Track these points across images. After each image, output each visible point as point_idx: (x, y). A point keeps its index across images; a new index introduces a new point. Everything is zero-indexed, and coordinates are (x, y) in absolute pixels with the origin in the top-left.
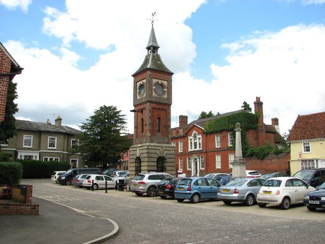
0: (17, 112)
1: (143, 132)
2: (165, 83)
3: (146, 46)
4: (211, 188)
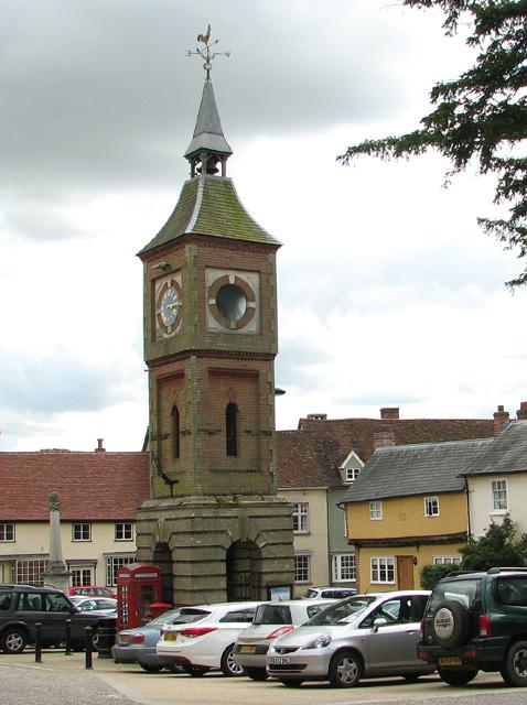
0: (396, 411)
1: (177, 455)
2: (252, 280)
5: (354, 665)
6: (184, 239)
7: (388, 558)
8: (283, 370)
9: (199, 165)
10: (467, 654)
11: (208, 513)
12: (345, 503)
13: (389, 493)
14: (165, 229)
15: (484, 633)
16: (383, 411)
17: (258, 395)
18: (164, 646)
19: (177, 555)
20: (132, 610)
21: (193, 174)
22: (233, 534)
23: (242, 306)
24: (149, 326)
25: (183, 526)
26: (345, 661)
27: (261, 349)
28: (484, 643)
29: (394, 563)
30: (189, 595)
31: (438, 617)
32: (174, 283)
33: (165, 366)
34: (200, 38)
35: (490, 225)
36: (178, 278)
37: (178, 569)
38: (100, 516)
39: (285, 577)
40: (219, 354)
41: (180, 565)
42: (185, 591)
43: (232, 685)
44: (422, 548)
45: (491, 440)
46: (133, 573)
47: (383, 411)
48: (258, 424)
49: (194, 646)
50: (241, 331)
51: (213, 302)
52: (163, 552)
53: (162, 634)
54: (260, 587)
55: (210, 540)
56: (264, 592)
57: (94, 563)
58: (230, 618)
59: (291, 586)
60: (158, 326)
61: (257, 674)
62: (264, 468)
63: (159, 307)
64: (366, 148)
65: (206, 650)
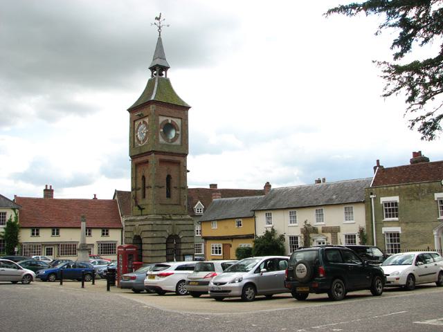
0: (216, 185)
1: (144, 197)
2: (178, 122)
3: (149, 66)
4: (426, 267)
5: (252, 291)
6: (150, 103)
7: (219, 244)
8: (191, 162)
9: (155, 72)
10: (313, 286)
11: (158, 222)
12: (201, 222)
13: (220, 218)
14: (134, 104)
15: (321, 275)
16: (211, 185)
17: (180, 172)
18: (148, 281)
19: (144, 241)
20: (125, 263)
21: (152, 76)
22: (169, 231)
23: (173, 133)
24: (132, 140)
25: (147, 228)
26: (249, 289)
27: (182, 152)
28: (322, 281)
29: (221, 247)
30: (150, 258)
31: (298, 268)
32: (144, 122)
33: (139, 158)
34: (156, 18)
35: (422, 44)
36: (147, 120)
37: (144, 247)
38: (96, 226)
39: (190, 251)
40: (164, 153)
41: (146, 245)
42: (148, 257)
43: (185, 300)
44: (234, 241)
45: (263, 196)
46: (125, 248)
47: (211, 185)
48: (180, 184)
49: (162, 282)
50: (174, 144)
51: (162, 130)
52: (138, 240)
53: (146, 275)
54: (180, 255)
55: (159, 234)
56: (182, 258)
57: (93, 245)
58: (179, 268)
59: (193, 255)
60: (136, 141)
61: (196, 294)
62: (182, 203)
63: (137, 132)
64: (335, 10)
65: (168, 283)
